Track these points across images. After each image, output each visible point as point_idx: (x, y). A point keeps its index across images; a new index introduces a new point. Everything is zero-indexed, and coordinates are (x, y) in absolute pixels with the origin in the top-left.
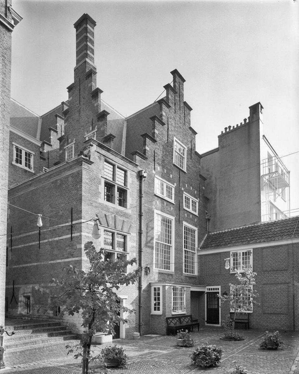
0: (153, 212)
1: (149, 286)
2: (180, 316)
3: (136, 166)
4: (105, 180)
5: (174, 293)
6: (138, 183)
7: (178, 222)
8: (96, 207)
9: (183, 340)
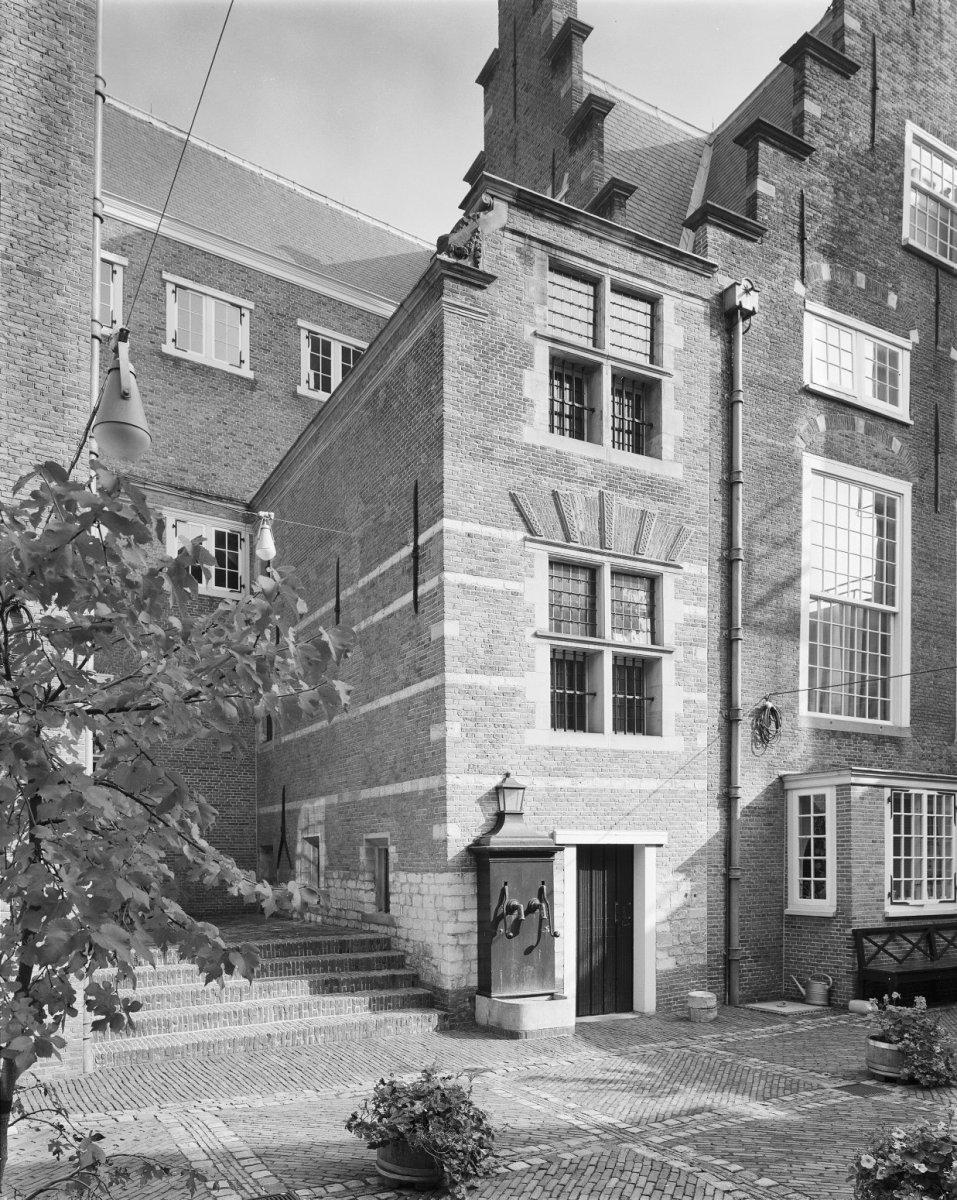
0: (797, 466)
1: (779, 789)
2: (929, 922)
3: (704, 269)
4: (551, 349)
5: (897, 820)
6: (717, 346)
7: (929, 506)
8: (510, 462)
9: (894, 1047)
